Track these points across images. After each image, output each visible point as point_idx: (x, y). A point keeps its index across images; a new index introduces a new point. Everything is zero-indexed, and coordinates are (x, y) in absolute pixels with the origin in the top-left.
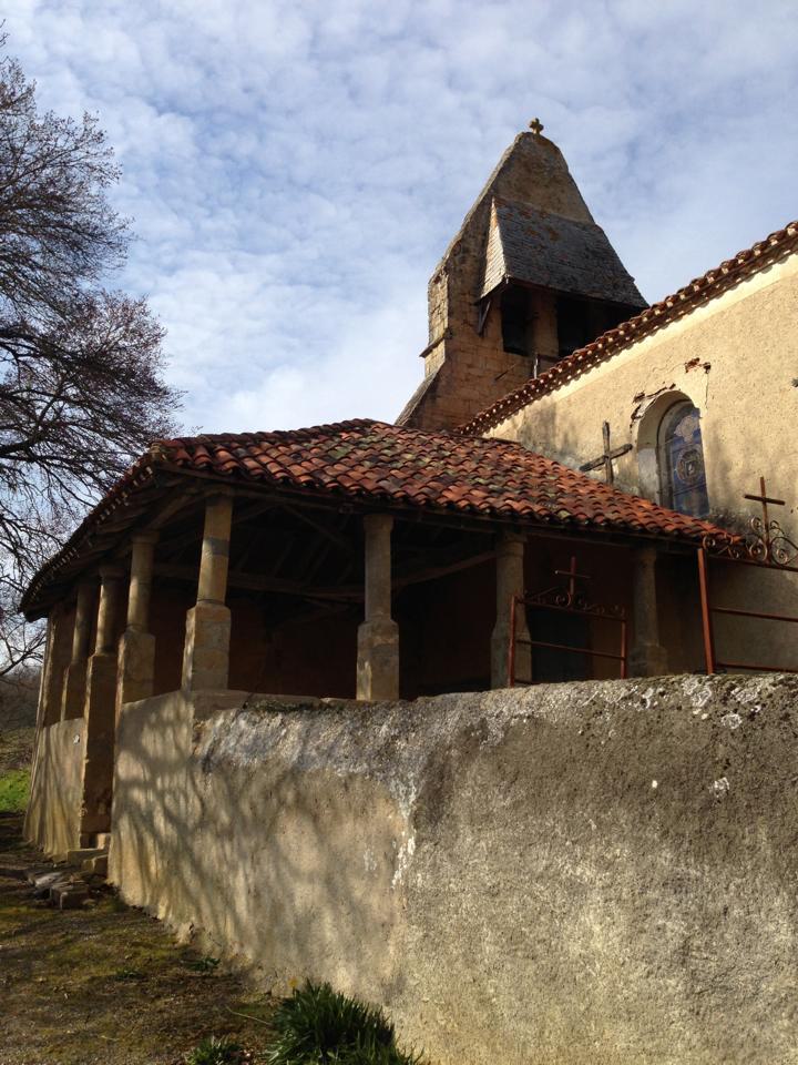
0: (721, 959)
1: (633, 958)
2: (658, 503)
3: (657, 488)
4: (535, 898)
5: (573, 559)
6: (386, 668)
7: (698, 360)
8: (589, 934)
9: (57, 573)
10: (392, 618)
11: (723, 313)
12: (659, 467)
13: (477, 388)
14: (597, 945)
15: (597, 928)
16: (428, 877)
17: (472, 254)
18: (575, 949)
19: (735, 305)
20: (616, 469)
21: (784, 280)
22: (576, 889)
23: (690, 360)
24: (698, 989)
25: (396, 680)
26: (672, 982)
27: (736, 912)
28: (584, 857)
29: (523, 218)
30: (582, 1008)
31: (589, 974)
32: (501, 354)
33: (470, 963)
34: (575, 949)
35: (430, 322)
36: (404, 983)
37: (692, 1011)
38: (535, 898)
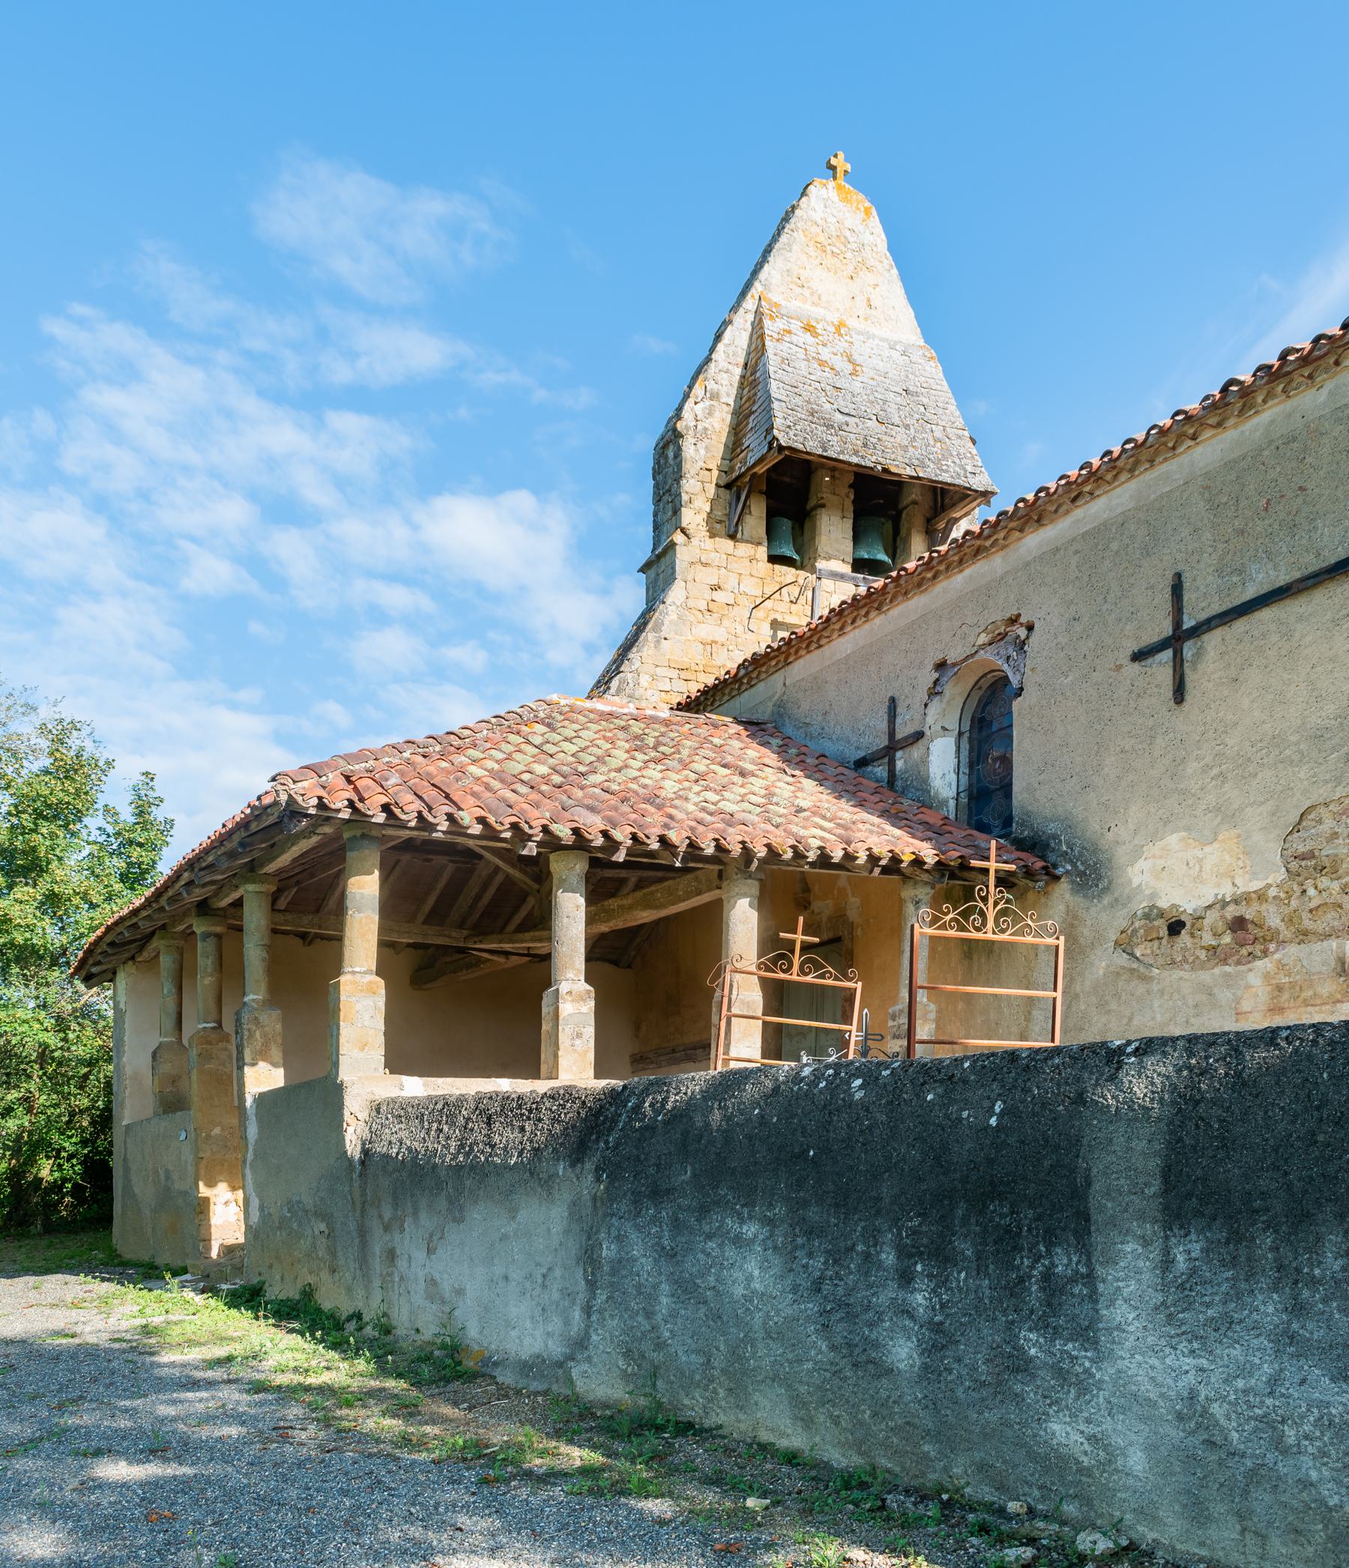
0: (846, 1284)
1: (783, 1292)
2: (952, 816)
3: (953, 793)
4: (708, 1255)
5: (801, 919)
6: (578, 1042)
7: (1019, 615)
8: (749, 1278)
9: (135, 926)
10: (587, 981)
11: (1058, 549)
12: (959, 762)
13: (725, 622)
14: (757, 1285)
15: (756, 1273)
16: (613, 1247)
17: (724, 399)
18: (739, 1291)
19: (1074, 540)
20: (900, 764)
21: (1137, 509)
22: (738, 1241)
23: (1008, 615)
24: (828, 1308)
25: (591, 1056)
26: (811, 1306)
27: (860, 1248)
28: (750, 1218)
29: (808, 338)
30: (742, 1335)
31: (749, 1309)
32: (763, 566)
33: (649, 1315)
34: (739, 1291)
35: (655, 515)
36: (589, 1339)
37: (823, 1325)
38: (708, 1255)
